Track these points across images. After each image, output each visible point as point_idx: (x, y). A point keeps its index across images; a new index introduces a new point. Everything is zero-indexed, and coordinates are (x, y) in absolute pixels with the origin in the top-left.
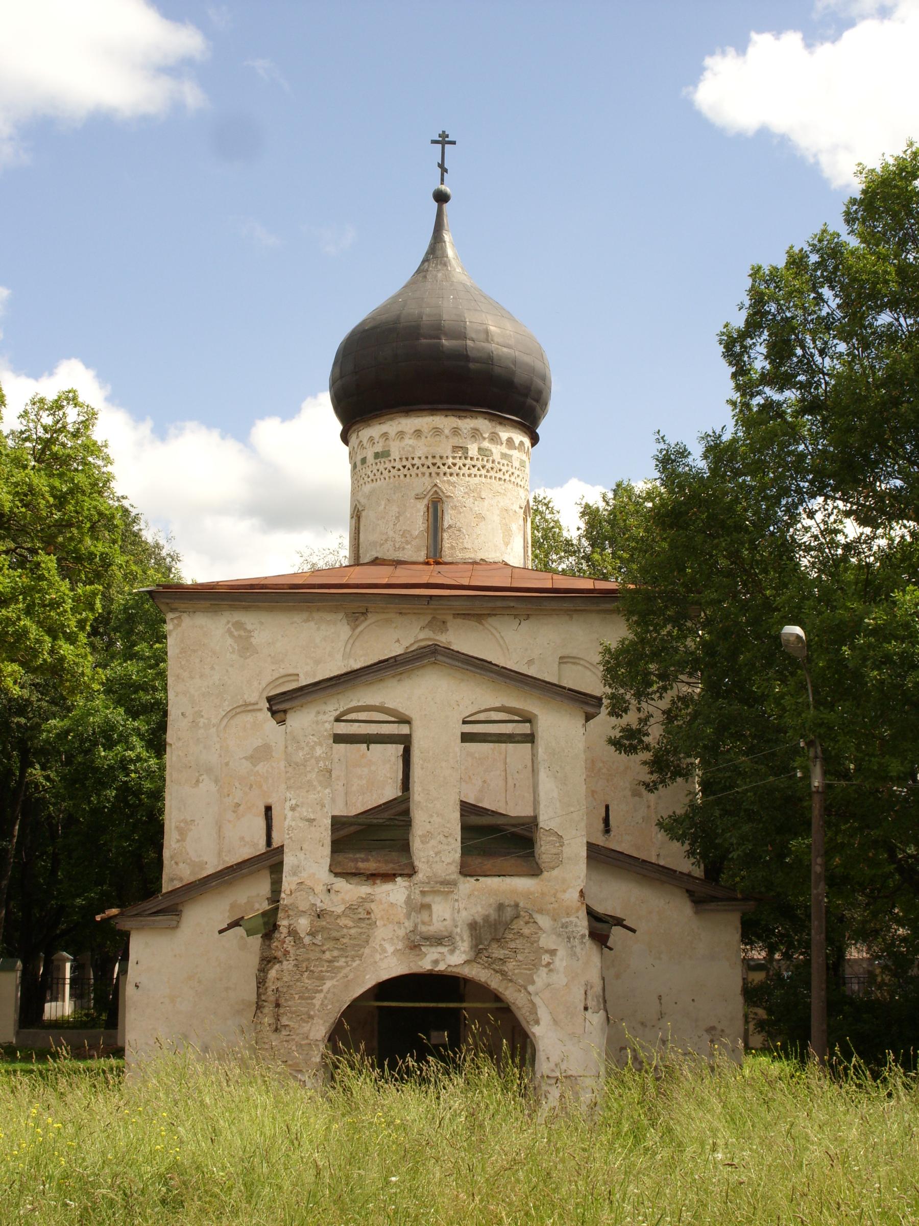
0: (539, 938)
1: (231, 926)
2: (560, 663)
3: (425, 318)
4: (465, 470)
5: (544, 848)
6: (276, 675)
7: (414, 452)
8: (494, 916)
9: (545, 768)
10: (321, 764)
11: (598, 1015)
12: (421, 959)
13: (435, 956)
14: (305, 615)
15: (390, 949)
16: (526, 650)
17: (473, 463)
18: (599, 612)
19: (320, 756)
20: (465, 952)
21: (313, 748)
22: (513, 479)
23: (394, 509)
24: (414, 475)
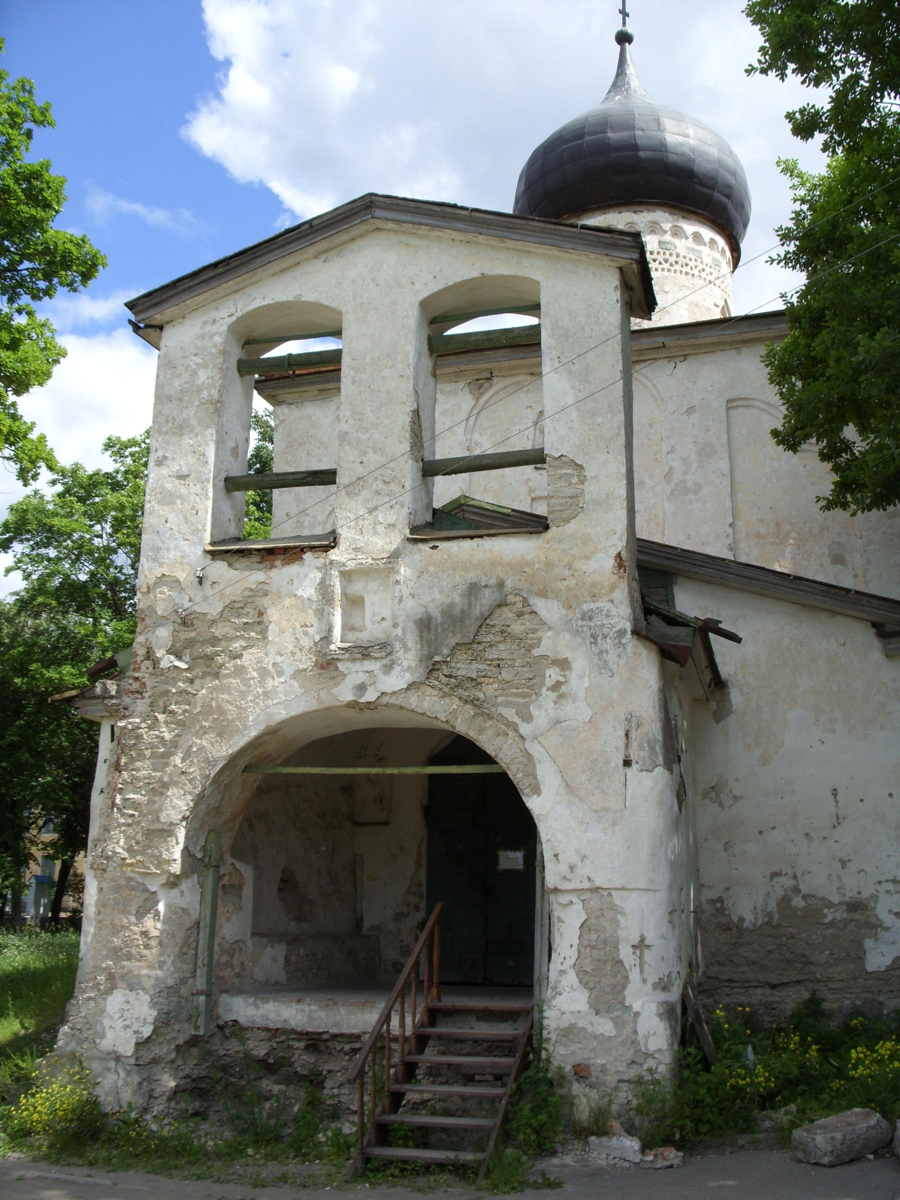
0: (539, 639)
2: (728, 408)
9: (551, 360)
10: (205, 394)
11: (653, 774)
12: (337, 685)
13: (361, 678)
16: (685, 396)
19: (203, 384)
20: (409, 668)
21: (194, 374)
22: (703, 275)
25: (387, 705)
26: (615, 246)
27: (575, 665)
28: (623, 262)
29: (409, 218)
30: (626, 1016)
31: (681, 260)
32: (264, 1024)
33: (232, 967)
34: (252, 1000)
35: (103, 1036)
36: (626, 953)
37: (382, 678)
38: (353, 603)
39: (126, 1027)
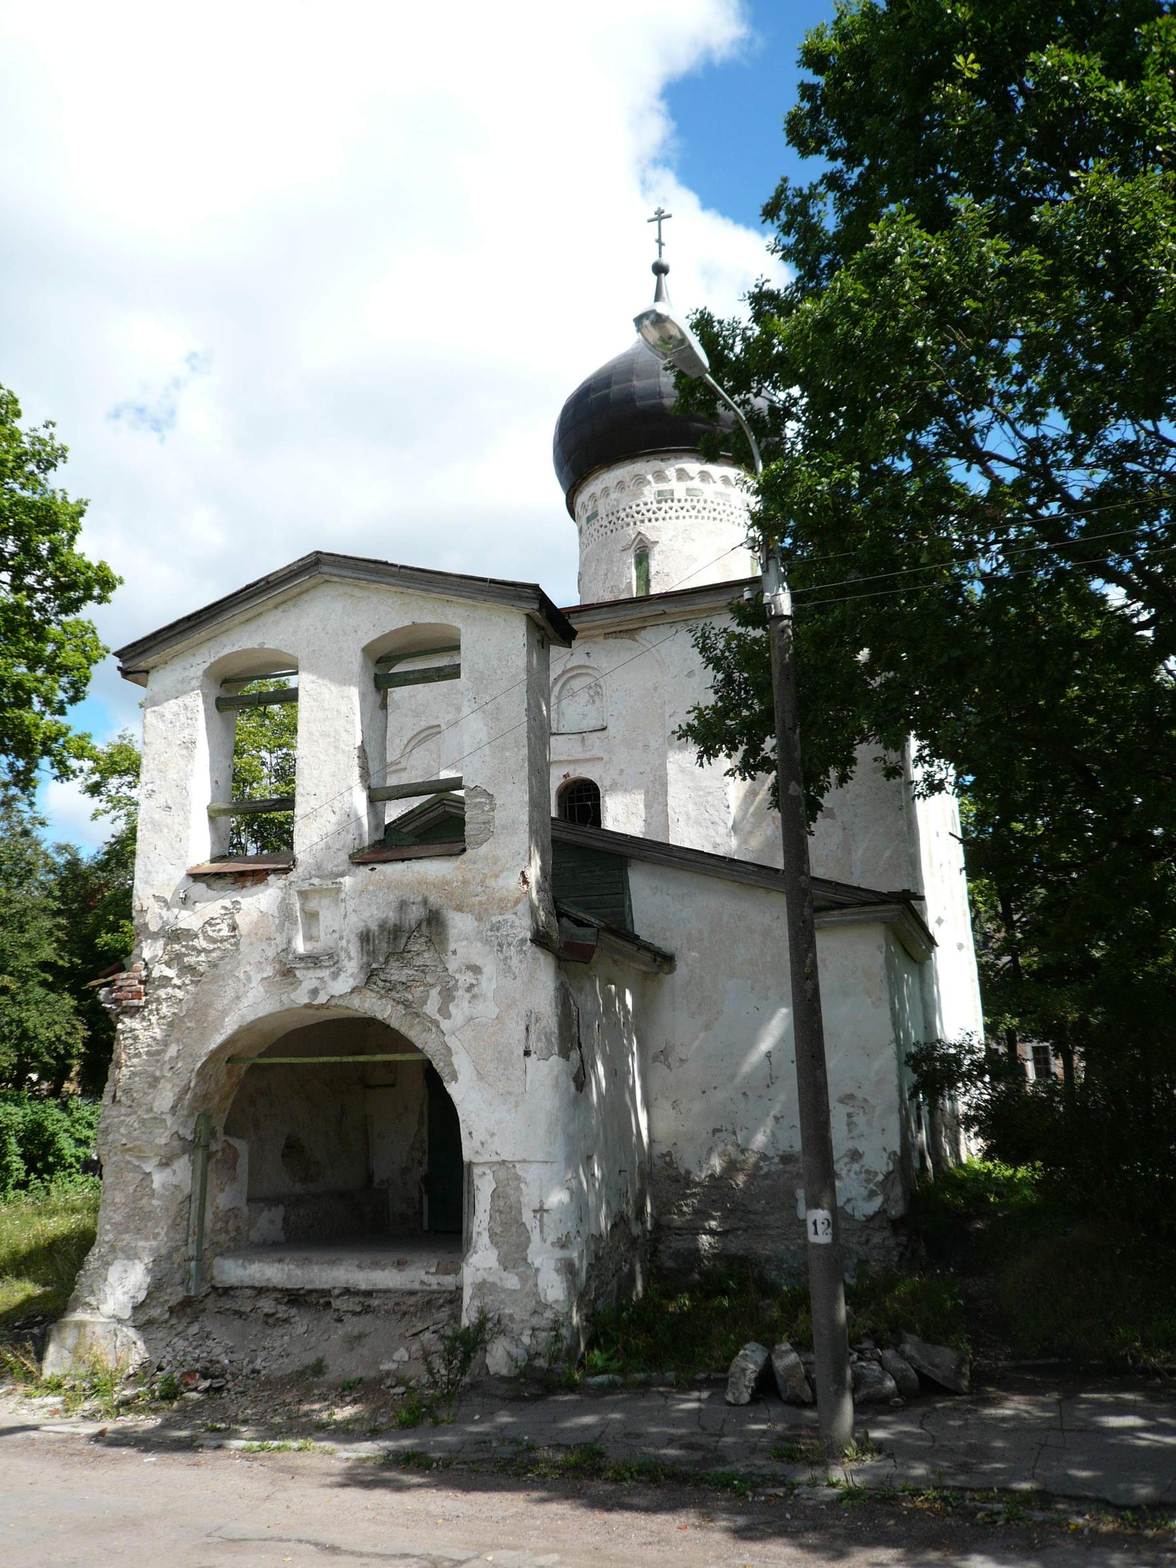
4: (672, 513)
6: (418, 729)
8: (392, 916)
12: (295, 990)
13: (314, 983)
17: (681, 504)
20: (351, 976)
22: (732, 518)
25: (336, 1006)
26: (520, 598)
27: (485, 970)
28: (528, 611)
29: (349, 573)
30: (529, 1272)
31: (709, 506)
32: (250, 1283)
33: (227, 1232)
34: (240, 1262)
36: (527, 1217)
37: (330, 983)
38: (311, 917)
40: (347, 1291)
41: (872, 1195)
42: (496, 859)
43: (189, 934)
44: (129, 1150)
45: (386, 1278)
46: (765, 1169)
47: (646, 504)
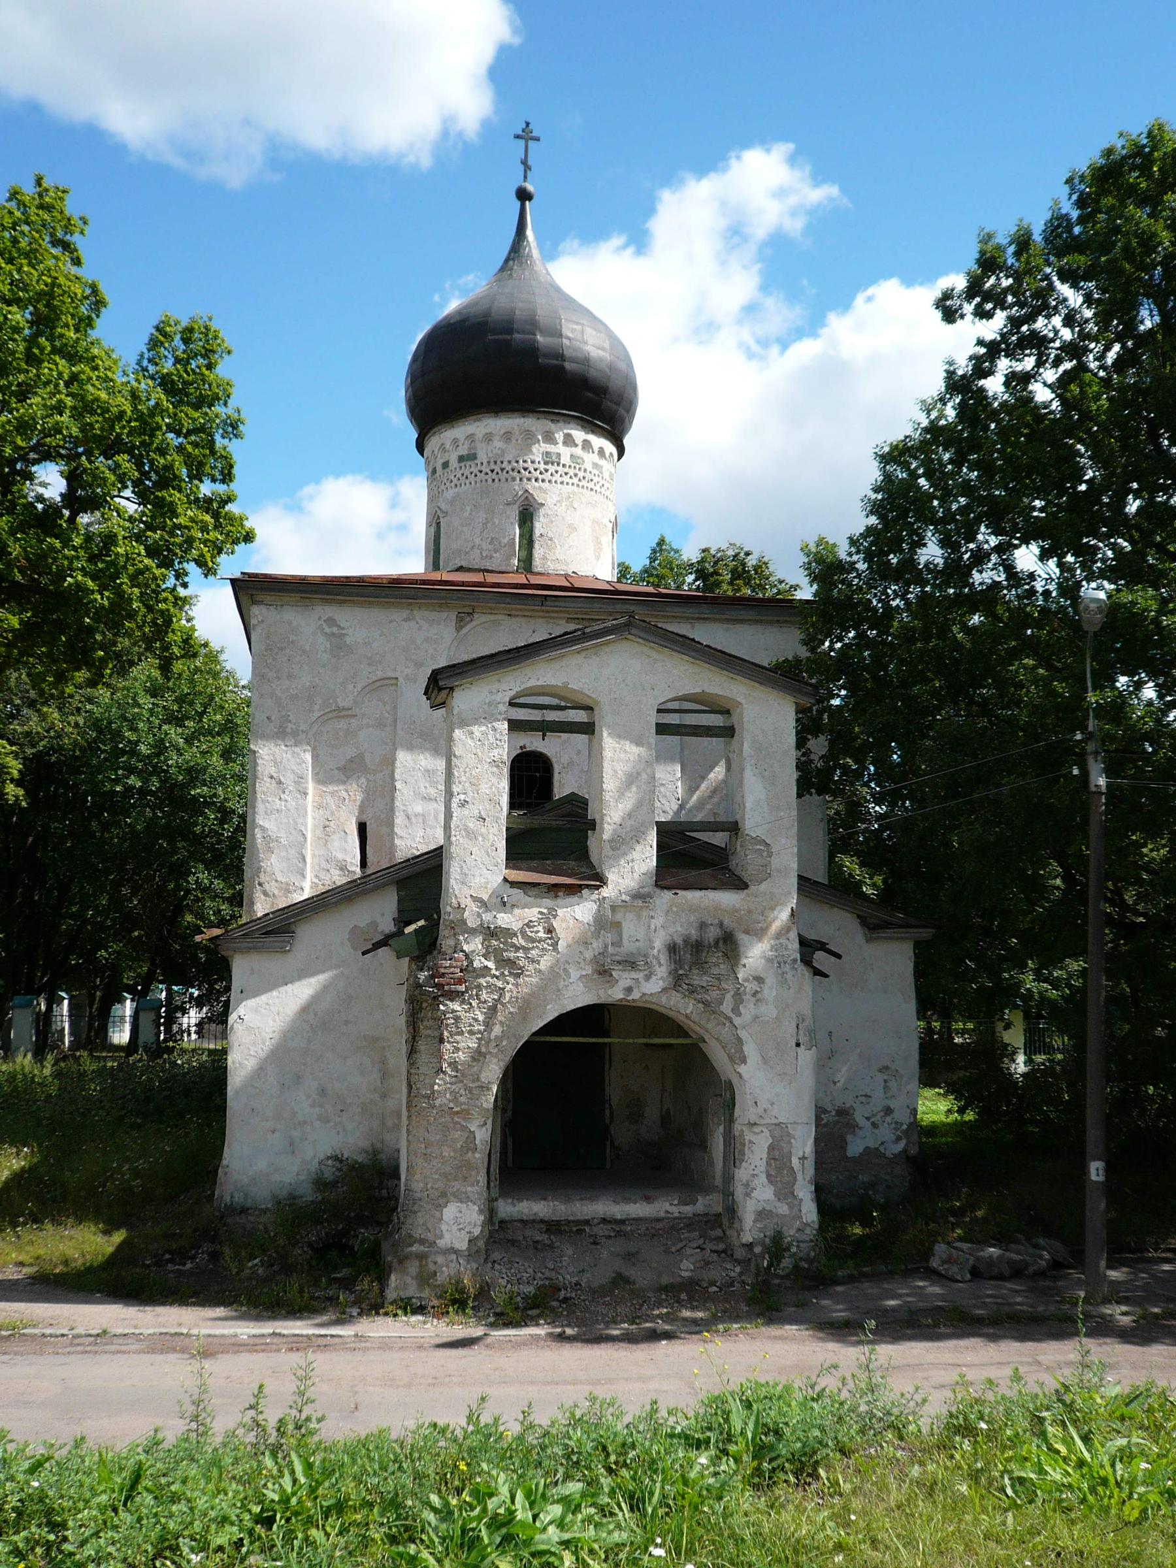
1: (377, 946)
3: (517, 312)
4: (557, 477)
5: (746, 861)
7: (503, 455)
8: (694, 934)
14: (405, 613)
15: (575, 974)
17: (566, 470)
18: (722, 621)
20: (661, 978)
22: (603, 490)
23: (481, 516)
24: (503, 480)
27: (767, 981)
31: (588, 475)
35: (441, 1237)
39: (460, 1230)
40: (604, 1221)
41: (899, 1139)
42: (772, 896)
43: (509, 933)
44: (458, 1113)
45: (638, 1209)
46: (825, 1121)
47: (533, 462)
